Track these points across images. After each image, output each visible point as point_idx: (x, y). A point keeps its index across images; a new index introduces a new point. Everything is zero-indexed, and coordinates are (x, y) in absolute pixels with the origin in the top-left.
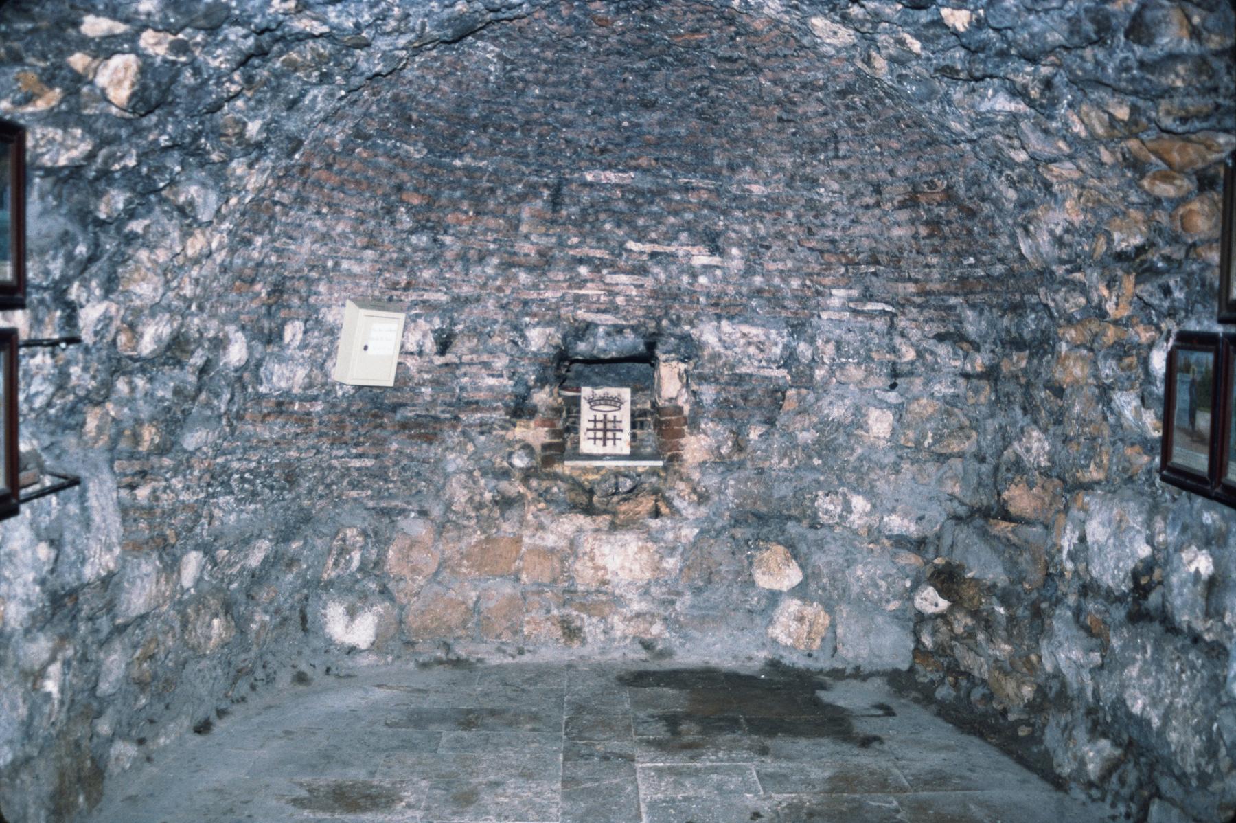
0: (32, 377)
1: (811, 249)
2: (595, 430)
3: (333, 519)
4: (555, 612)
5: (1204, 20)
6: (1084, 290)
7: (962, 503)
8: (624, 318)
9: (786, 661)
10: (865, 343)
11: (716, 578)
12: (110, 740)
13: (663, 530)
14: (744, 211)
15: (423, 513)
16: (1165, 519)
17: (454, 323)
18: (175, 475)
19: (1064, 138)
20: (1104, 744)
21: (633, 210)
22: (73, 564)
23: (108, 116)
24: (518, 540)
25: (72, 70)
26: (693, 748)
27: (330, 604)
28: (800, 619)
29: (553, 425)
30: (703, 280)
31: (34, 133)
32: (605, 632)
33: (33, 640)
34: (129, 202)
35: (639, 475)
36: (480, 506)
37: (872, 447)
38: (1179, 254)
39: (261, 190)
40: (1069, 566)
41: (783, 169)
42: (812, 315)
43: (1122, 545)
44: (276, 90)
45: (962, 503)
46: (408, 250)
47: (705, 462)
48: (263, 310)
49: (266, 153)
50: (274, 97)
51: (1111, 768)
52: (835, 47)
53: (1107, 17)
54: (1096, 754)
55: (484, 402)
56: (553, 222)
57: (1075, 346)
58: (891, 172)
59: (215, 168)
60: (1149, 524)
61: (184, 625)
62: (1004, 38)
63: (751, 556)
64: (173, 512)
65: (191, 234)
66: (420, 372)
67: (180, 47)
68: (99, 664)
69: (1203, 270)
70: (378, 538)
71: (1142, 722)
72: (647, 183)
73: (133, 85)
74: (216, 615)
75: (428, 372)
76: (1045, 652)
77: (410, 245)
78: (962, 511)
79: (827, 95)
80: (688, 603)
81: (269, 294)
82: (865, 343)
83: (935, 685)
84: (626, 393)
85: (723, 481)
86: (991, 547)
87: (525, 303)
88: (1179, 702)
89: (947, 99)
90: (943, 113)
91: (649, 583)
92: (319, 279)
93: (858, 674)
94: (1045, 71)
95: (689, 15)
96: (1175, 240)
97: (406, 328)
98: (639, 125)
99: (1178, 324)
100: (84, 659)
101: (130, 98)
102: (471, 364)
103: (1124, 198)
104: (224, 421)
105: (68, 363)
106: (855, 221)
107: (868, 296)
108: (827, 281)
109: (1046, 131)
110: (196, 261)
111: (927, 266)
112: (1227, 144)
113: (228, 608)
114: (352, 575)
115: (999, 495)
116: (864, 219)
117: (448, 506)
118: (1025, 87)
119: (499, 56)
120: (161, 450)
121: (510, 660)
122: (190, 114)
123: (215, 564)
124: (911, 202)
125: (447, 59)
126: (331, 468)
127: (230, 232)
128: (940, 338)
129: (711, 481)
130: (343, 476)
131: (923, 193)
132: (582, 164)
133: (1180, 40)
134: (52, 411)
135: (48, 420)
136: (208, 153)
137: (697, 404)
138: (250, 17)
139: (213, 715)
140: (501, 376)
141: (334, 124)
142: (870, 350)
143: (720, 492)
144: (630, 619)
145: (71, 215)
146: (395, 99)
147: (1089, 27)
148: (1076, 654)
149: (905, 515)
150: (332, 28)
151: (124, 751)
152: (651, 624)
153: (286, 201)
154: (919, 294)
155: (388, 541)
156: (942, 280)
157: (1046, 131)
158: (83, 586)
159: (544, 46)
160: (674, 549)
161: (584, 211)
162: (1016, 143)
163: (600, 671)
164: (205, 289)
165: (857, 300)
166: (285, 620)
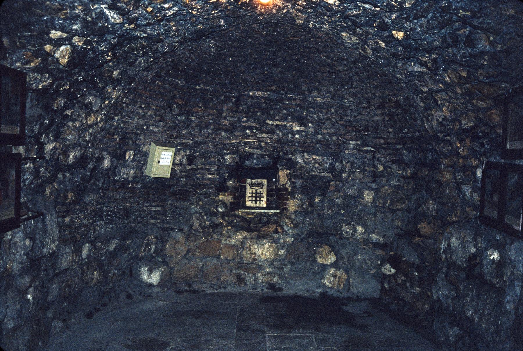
0: (25, 172)
1: (341, 124)
2: (252, 197)
3: (143, 232)
4: (234, 272)
5: (495, 38)
6: (451, 144)
7: (401, 230)
8: (265, 151)
9: (328, 294)
10: (363, 163)
11: (300, 259)
12: (52, 320)
13: (279, 239)
14: (314, 109)
15: (181, 230)
16: (481, 237)
17: (195, 152)
18: (80, 213)
19: (442, 83)
20: (456, 329)
21: (268, 108)
22: (39, 248)
23: (59, 69)
24: (220, 242)
25: (46, 51)
26: (290, 328)
27: (142, 266)
28: (335, 276)
29: (234, 195)
30: (297, 136)
31: (29, 76)
32: (255, 280)
33: (22, 278)
34: (65, 103)
35: (270, 216)
36: (204, 228)
37: (366, 206)
38: (487, 131)
39: (117, 98)
40: (444, 256)
41: (330, 92)
42: (342, 151)
43: (464, 247)
44: (125, 59)
45: (401, 230)
46: (177, 122)
47: (297, 211)
48: (118, 146)
49: (120, 83)
50: (124, 61)
51: (459, 338)
52: (350, 44)
53: (457, 36)
54: (453, 333)
55: (207, 185)
56: (236, 112)
57: (447, 166)
58: (374, 94)
59: (100, 89)
60: (475, 239)
61: (83, 272)
62: (417, 43)
63: (315, 251)
64: (80, 227)
65: (90, 116)
66: (181, 172)
67: (87, 43)
68: (48, 288)
69: (497, 137)
70: (162, 240)
71: (471, 320)
72: (275, 97)
73: (69, 57)
74: (95, 270)
75: (184, 172)
76: (434, 291)
77: (178, 120)
78: (401, 233)
79: (348, 63)
80: (289, 269)
81: (120, 139)
82: (363, 163)
83: (387, 304)
84: (265, 182)
85: (305, 219)
86: (413, 248)
87: (224, 144)
88: (486, 312)
89: (395, 66)
90: (394, 71)
91: (273, 260)
92: (141, 134)
93: (359, 299)
94: (434, 56)
95: (292, 30)
96: (486, 124)
97: (175, 154)
98: (272, 73)
99: (487, 158)
100: (42, 286)
101: (68, 62)
102: (202, 169)
103: (467, 107)
104: (101, 191)
105: (40, 167)
106: (360, 114)
107: (364, 144)
108: (348, 138)
109: (435, 80)
110: (91, 126)
111: (388, 132)
112: (505, 87)
113: (100, 267)
114: (151, 254)
115: (417, 226)
116: (363, 113)
117: (191, 226)
118: (426, 62)
119: (215, 44)
120: (75, 202)
121: (215, 291)
122: (91, 68)
123: (96, 249)
124: (381, 106)
125: (194, 46)
126: (144, 210)
127: (105, 115)
128: (394, 162)
129: (299, 219)
130: (148, 214)
131: (387, 103)
132: (248, 88)
133: (486, 46)
134: (33, 186)
135: (31, 188)
136: (97, 83)
137: (294, 187)
138: (116, 31)
139: (93, 310)
140: (214, 174)
141: (148, 72)
142: (365, 166)
143: (303, 223)
144: (265, 275)
145: (41, 108)
146: (173, 61)
147: (450, 40)
148: (446, 292)
149: (378, 234)
150: (148, 34)
151: (58, 324)
152: (274, 277)
153: (128, 102)
154: (385, 144)
155: (166, 241)
156: (394, 138)
157: (435, 80)
158: (43, 256)
159: (233, 41)
160: (284, 246)
161: (249, 108)
162: (423, 84)
163: (253, 296)
164: (94, 138)
165: (360, 146)
166: (124, 273)
